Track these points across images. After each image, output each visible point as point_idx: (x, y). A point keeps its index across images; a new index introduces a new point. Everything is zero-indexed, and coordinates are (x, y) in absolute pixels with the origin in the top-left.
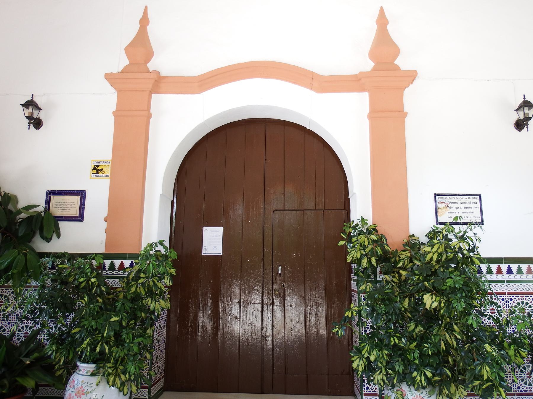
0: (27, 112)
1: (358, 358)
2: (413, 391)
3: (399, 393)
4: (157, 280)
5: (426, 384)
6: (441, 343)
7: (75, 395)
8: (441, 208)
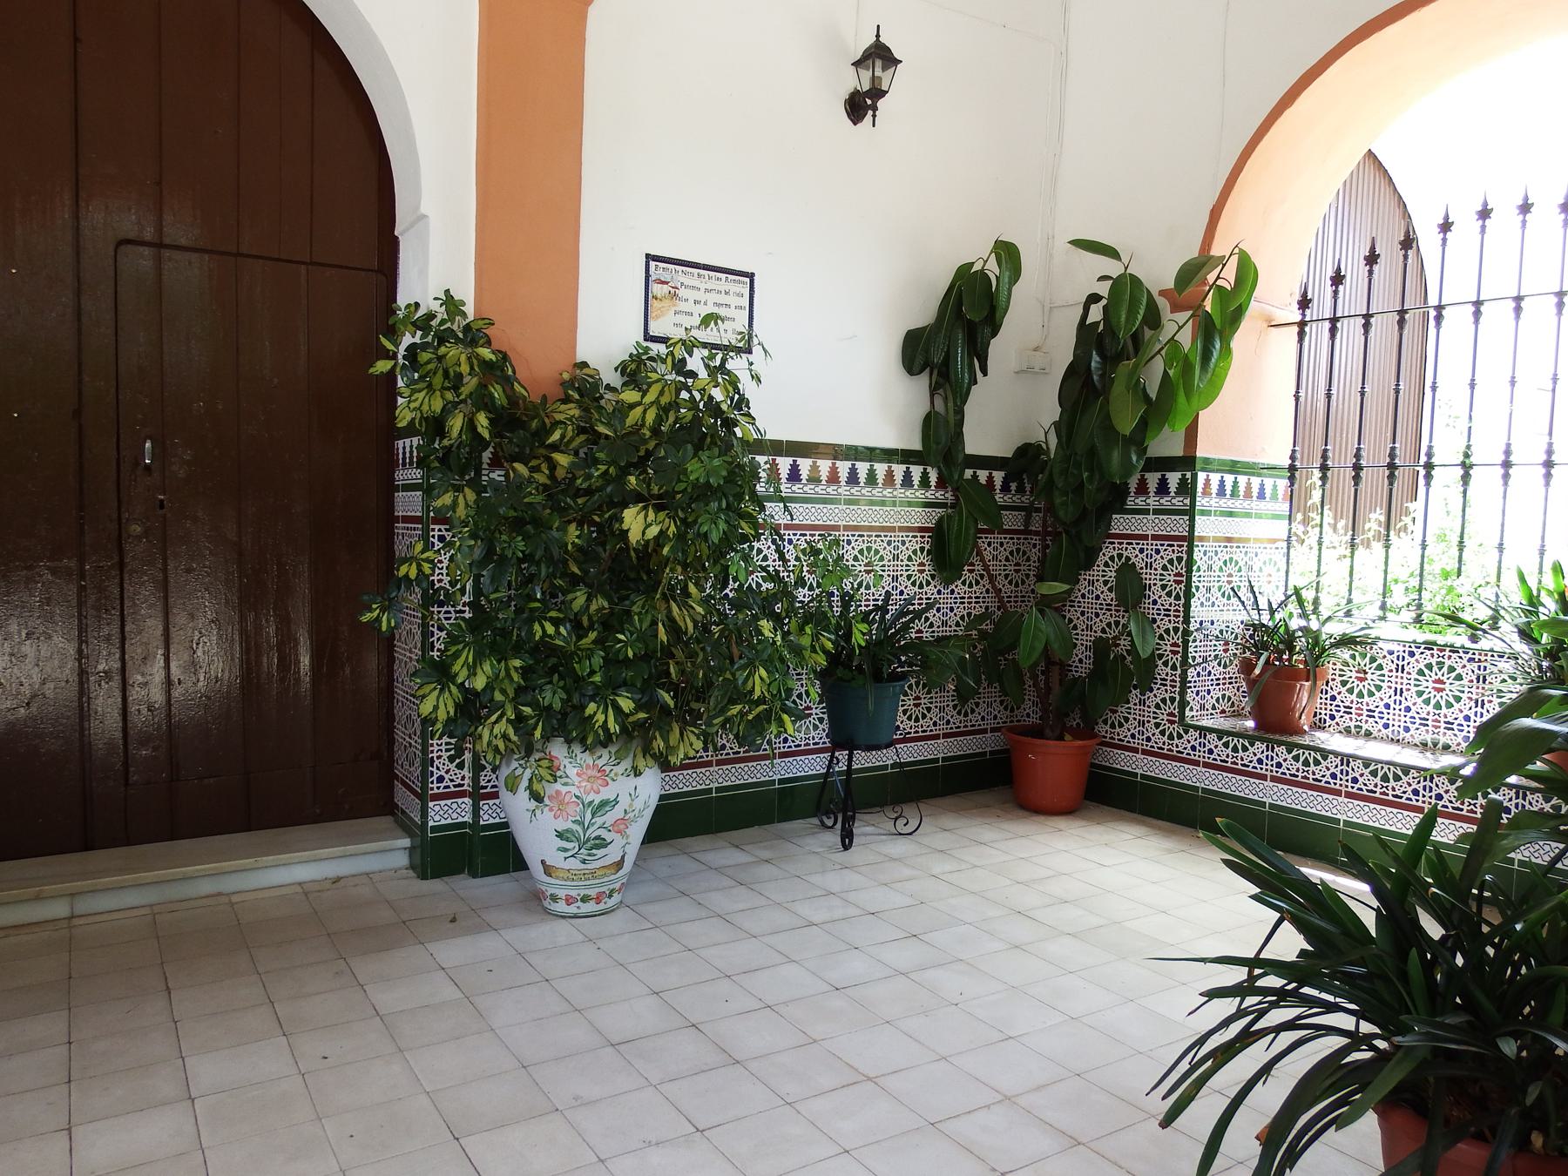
1: (435, 689)
2: (578, 753)
3: (545, 763)
5: (617, 728)
6: (657, 630)
8: (659, 296)
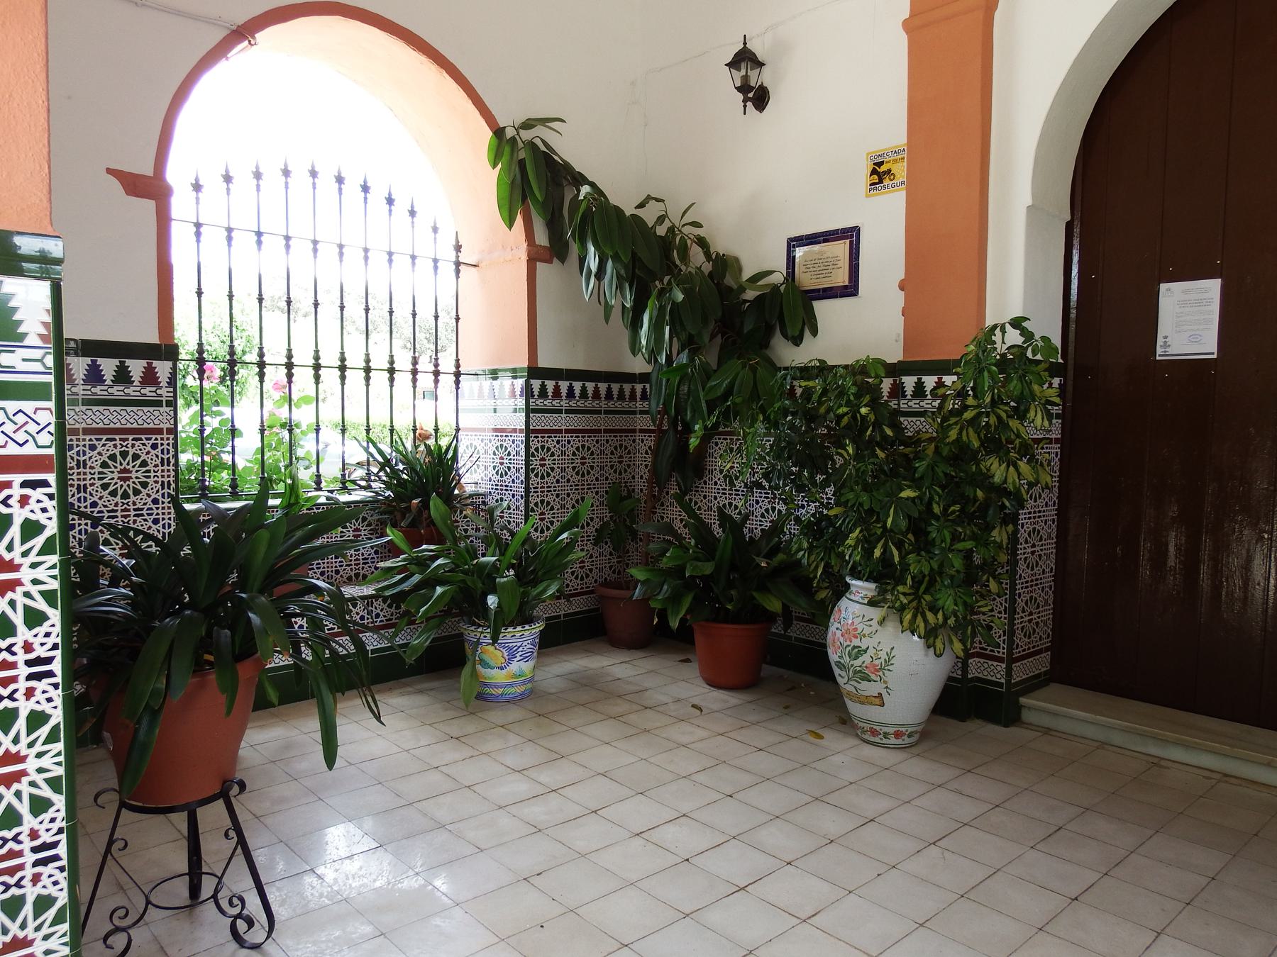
0: (738, 75)
4: (1007, 414)
7: (842, 635)
